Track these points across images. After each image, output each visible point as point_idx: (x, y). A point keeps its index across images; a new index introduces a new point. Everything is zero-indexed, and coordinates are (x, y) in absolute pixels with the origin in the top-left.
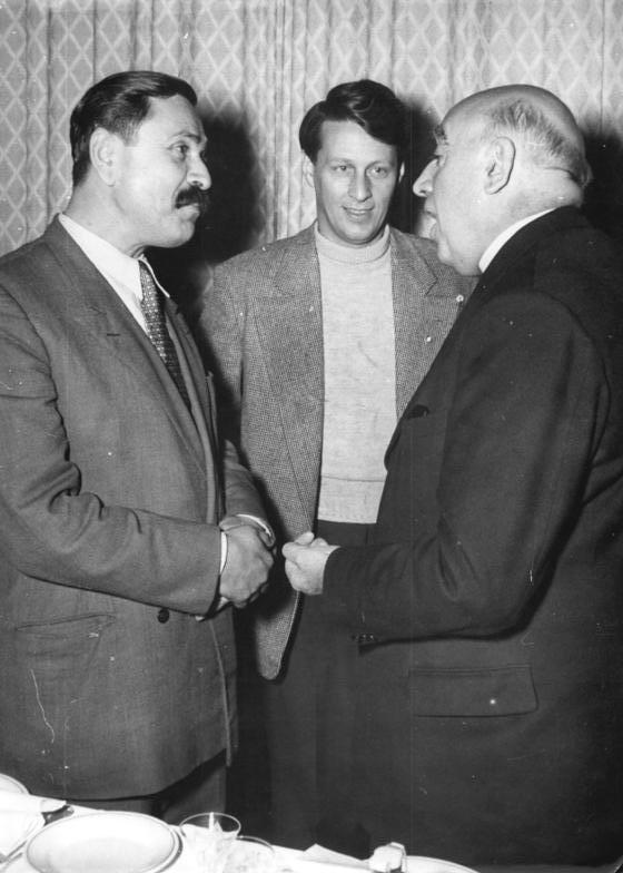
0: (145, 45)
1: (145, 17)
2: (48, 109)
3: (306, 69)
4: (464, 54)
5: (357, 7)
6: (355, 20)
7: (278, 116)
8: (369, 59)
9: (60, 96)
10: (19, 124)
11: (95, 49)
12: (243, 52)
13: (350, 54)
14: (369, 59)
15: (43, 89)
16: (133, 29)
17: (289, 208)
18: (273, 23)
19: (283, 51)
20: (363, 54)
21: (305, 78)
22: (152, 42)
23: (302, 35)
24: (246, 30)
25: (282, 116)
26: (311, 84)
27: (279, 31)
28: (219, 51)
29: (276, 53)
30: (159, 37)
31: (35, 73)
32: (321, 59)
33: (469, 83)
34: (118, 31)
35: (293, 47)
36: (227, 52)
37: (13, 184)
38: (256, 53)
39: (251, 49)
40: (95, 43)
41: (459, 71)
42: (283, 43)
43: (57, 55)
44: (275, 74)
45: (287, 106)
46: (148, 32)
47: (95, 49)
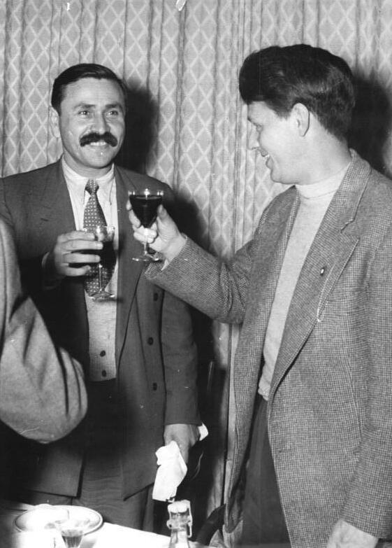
0: (155, 67)
1: (158, 21)
2: (94, 54)
3: (262, 25)
4: (365, 15)
5: (296, 14)
6: (295, 23)
7: (238, 114)
8: (304, 19)
9: (102, 47)
10: (74, 39)
11: (126, 16)
12: (212, 156)
13: (292, 17)
14: (304, 19)
15: (91, 42)
16: (150, 28)
17: (246, 178)
18: (237, 22)
19: (243, 40)
20: (301, 16)
21: (261, 31)
22: (163, 10)
23: (257, 32)
24: (218, 29)
25: (241, 114)
26: (265, 36)
27: (241, 28)
28: (200, 43)
29: (238, 42)
30: (165, 32)
31: (86, 31)
32: (273, 20)
33: (369, 35)
34: (141, 30)
35: (250, 38)
36: (197, 168)
37: (70, 54)
38: (225, 43)
39: (219, 96)
40: (127, 12)
41: (362, 27)
42: (244, 36)
43: (101, 19)
44: (237, 56)
45: (242, 194)
46: (158, 57)
47: (126, 16)
